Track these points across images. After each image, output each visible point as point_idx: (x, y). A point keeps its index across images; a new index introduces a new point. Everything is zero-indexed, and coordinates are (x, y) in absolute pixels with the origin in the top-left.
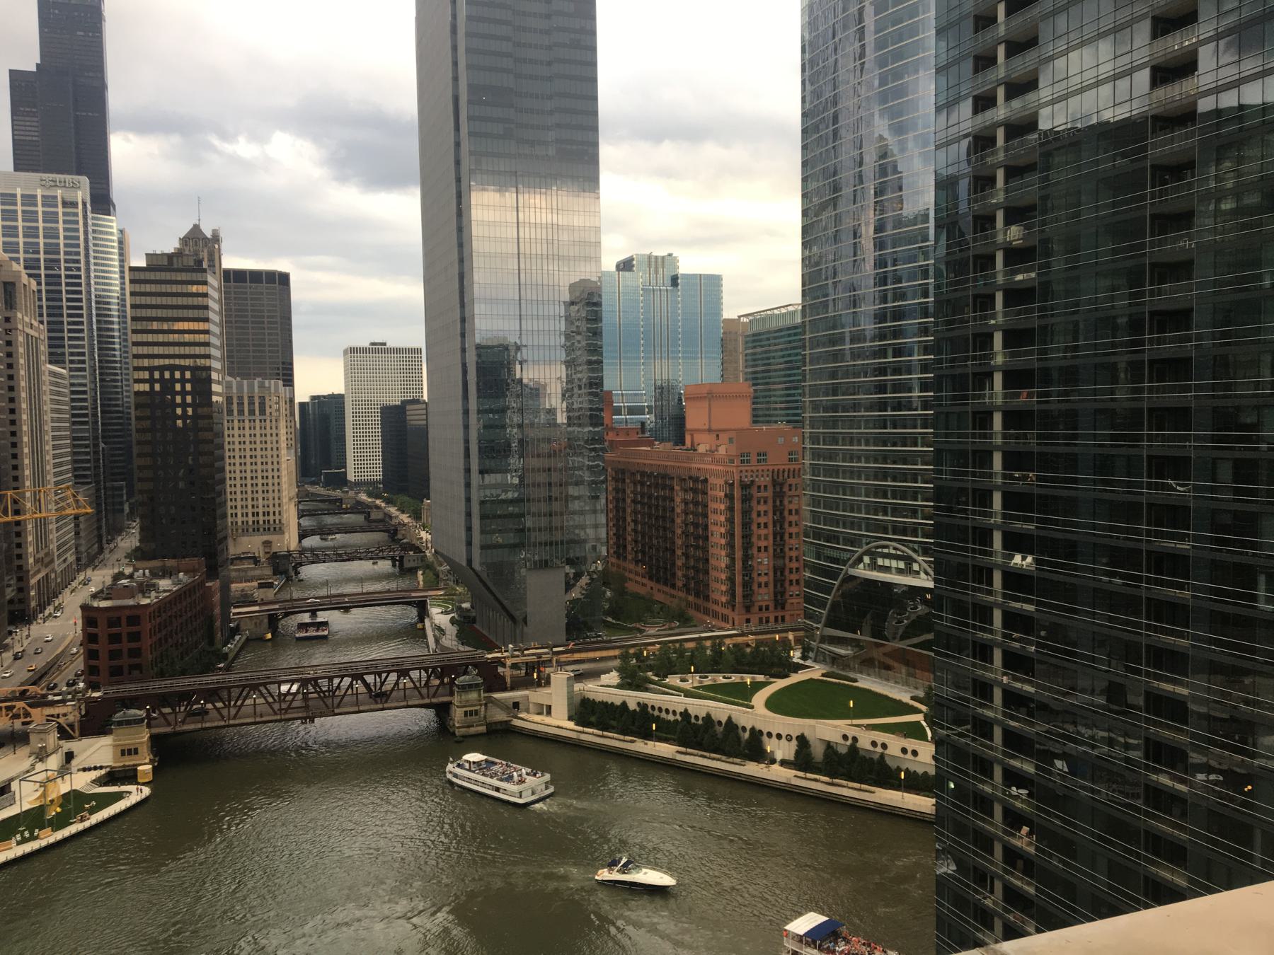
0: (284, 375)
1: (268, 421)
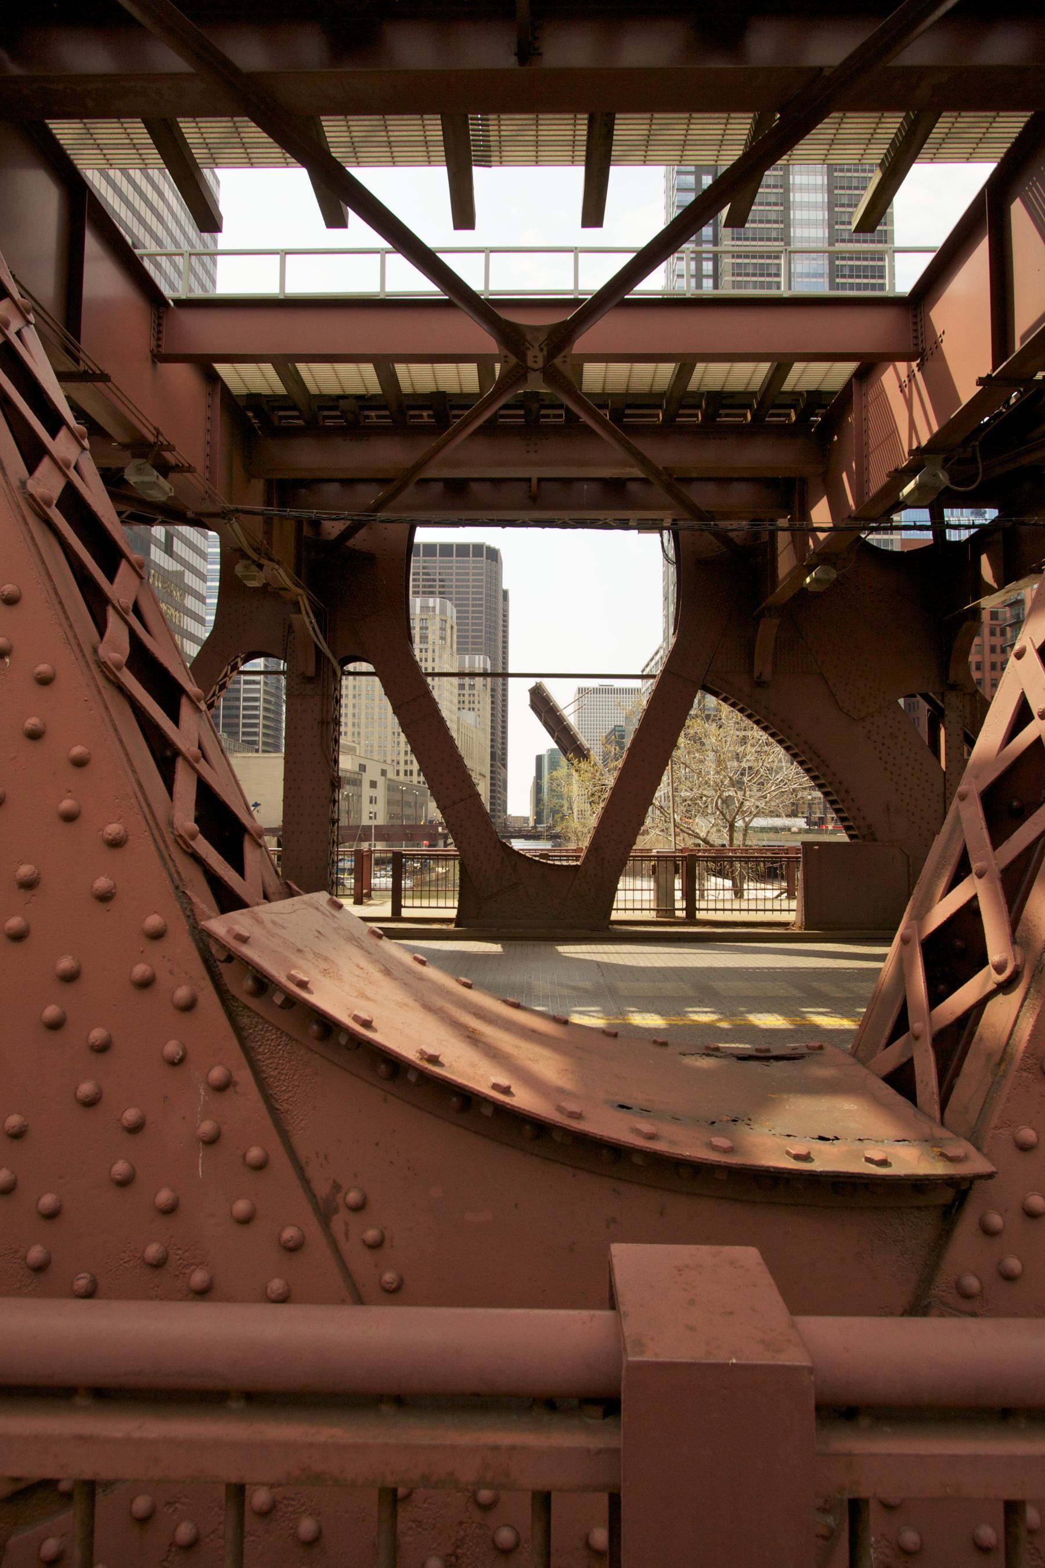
0: (440, 593)
1: (430, 651)
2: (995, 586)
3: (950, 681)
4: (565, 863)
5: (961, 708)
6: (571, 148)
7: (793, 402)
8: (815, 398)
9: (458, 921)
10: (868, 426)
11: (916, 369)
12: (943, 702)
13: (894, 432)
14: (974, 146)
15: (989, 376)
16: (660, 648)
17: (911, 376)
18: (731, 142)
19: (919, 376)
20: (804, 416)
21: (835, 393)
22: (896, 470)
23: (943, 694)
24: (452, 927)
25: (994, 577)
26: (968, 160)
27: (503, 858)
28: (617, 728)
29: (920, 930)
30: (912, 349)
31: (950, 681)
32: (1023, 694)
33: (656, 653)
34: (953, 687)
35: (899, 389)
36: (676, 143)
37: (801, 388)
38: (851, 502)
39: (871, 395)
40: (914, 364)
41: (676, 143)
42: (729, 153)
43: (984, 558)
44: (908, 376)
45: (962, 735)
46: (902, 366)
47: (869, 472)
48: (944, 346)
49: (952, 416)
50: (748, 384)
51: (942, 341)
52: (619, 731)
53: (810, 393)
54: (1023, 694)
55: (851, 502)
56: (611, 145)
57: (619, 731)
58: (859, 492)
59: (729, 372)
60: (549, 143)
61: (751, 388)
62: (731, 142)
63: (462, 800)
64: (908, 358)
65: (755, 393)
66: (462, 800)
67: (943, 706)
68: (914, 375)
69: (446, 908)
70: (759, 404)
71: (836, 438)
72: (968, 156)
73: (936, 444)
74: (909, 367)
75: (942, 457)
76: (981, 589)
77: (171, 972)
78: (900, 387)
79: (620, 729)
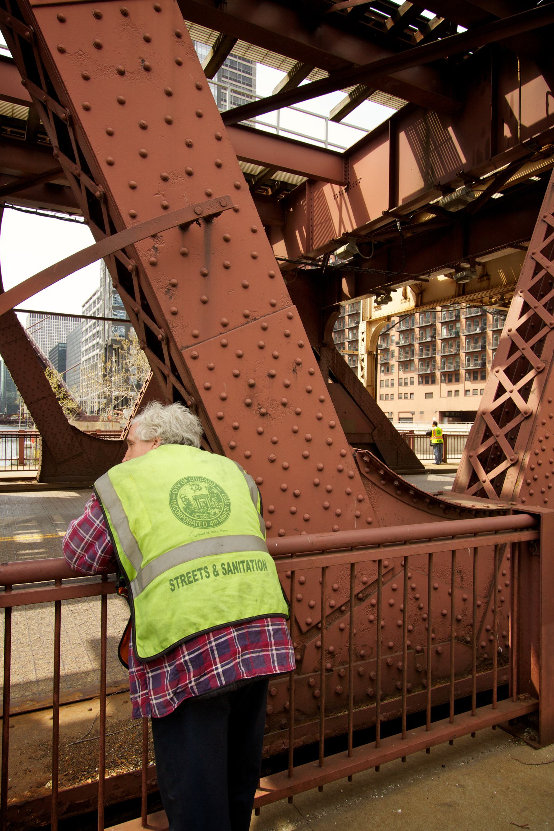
2: (350, 296)
3: (324, 341)
4: (114, 439)
5: (328, 356)
6: (208, 36)
7: (271, 185)
8: (284, 185)
9: (41, 480)
10: (313, 209)
11: (344, 191)
12: (320, 352)
13: (329, 219)
14: (388, 100)
15: (388, 211)
16: (97, 291)
17: (341, 193)
18: (288, 63)
19: (345, 194)
20: (276, 194)
21: (295, 185)
22: (333, 240)
23: (320, 348)
24: (34, 482)
25: (349, 292)
26: (383, 104)
27: (72, 436)
28: (60, 345)
29: (476, 453)
30: (344, 180)
31: (324, 341)
32: (500, 383)
33: (94, 295)
34: (325, 345)
35: (334, 198)
36: (262, 53)
37: (276, 179)
38: (301, 248)
39: (316, 194)
40: (343, 188)
41: (262, 53)
42: (285, 66)
43: (344, 280)
44: (339, 192)
45: (328, 372)
46: (337, 188)
47: (313, 234)
48: (361, 185)
49: (367, 223)
50: (253, 170)
51: (360, 182)
52: (62, 347)
53: (282, 182)
54: (500, 383)
55: (301, 248)
56: (234, 44)
57: (62, 347)
58: (308, 243)
59: (254, 169)
60: (197, 30)
61: (253, 173)
62: (288, 63)
63: (43, 398)
64: (341, 184)
65: (254, 176)
66: (43, 398)
67: (319, 355)
68: (343, 193)
69: (5, 471)
70: (256, 183)
71: (292, 210)
72: (384, 103)
73: (354, 234)
74: (341, 189)
75: (356, 239)
76: (342, 297)
77: (347, 467)
78: (334, 196)
79: (63, 345)
